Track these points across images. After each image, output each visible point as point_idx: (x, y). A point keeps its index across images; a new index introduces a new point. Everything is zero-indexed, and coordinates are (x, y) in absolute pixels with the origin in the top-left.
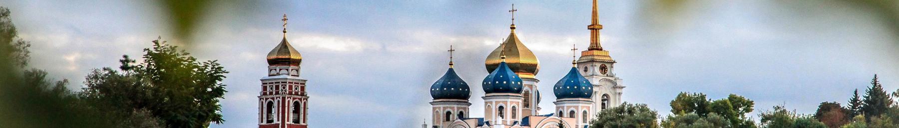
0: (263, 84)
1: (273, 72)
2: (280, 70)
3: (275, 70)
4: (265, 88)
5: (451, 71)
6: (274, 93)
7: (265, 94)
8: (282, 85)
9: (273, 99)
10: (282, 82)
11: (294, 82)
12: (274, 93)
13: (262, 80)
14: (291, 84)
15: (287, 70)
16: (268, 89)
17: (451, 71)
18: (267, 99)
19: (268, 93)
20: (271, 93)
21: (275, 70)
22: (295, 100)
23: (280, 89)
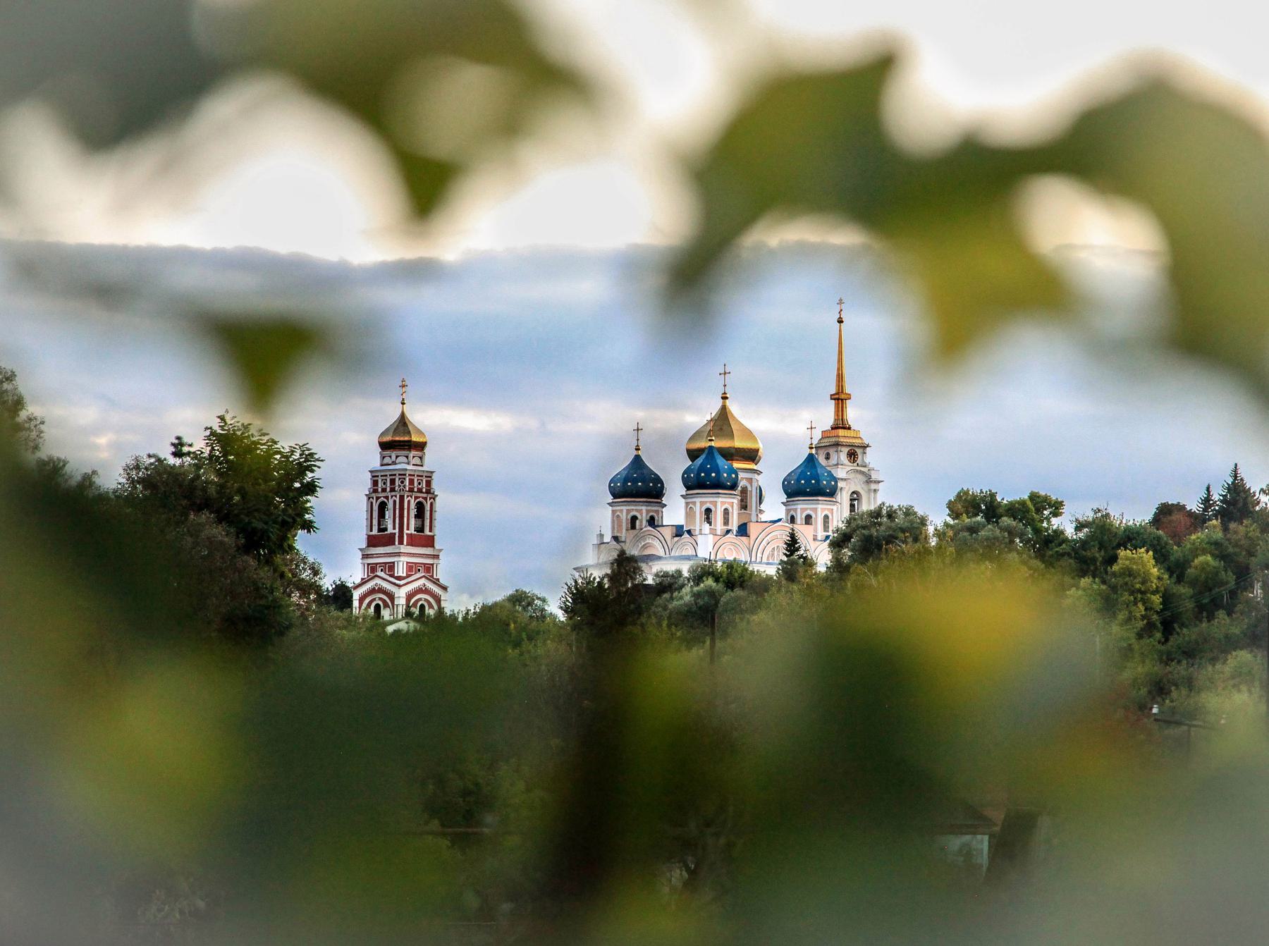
0: (373, 477)
1: (387, 460)
2: (397, 457)
3: (390, 457)
4: (375, 483)
5: (637, 459)
6: (388, 489)
7: (375, 491)
8: (399, 479)
9: (387, 498)
10: (400, 475)
11: (416, 474)
12: (388, 489)
13: (371, 472)
14: (412, 477)
15: (407, 457)
16: (380, 484)
17: (637, 459)
18: (378, 498)
19: (380, 490)
20: (384, 490)
21: (390, 457)
22: (418, 500)
23: (397, 484)
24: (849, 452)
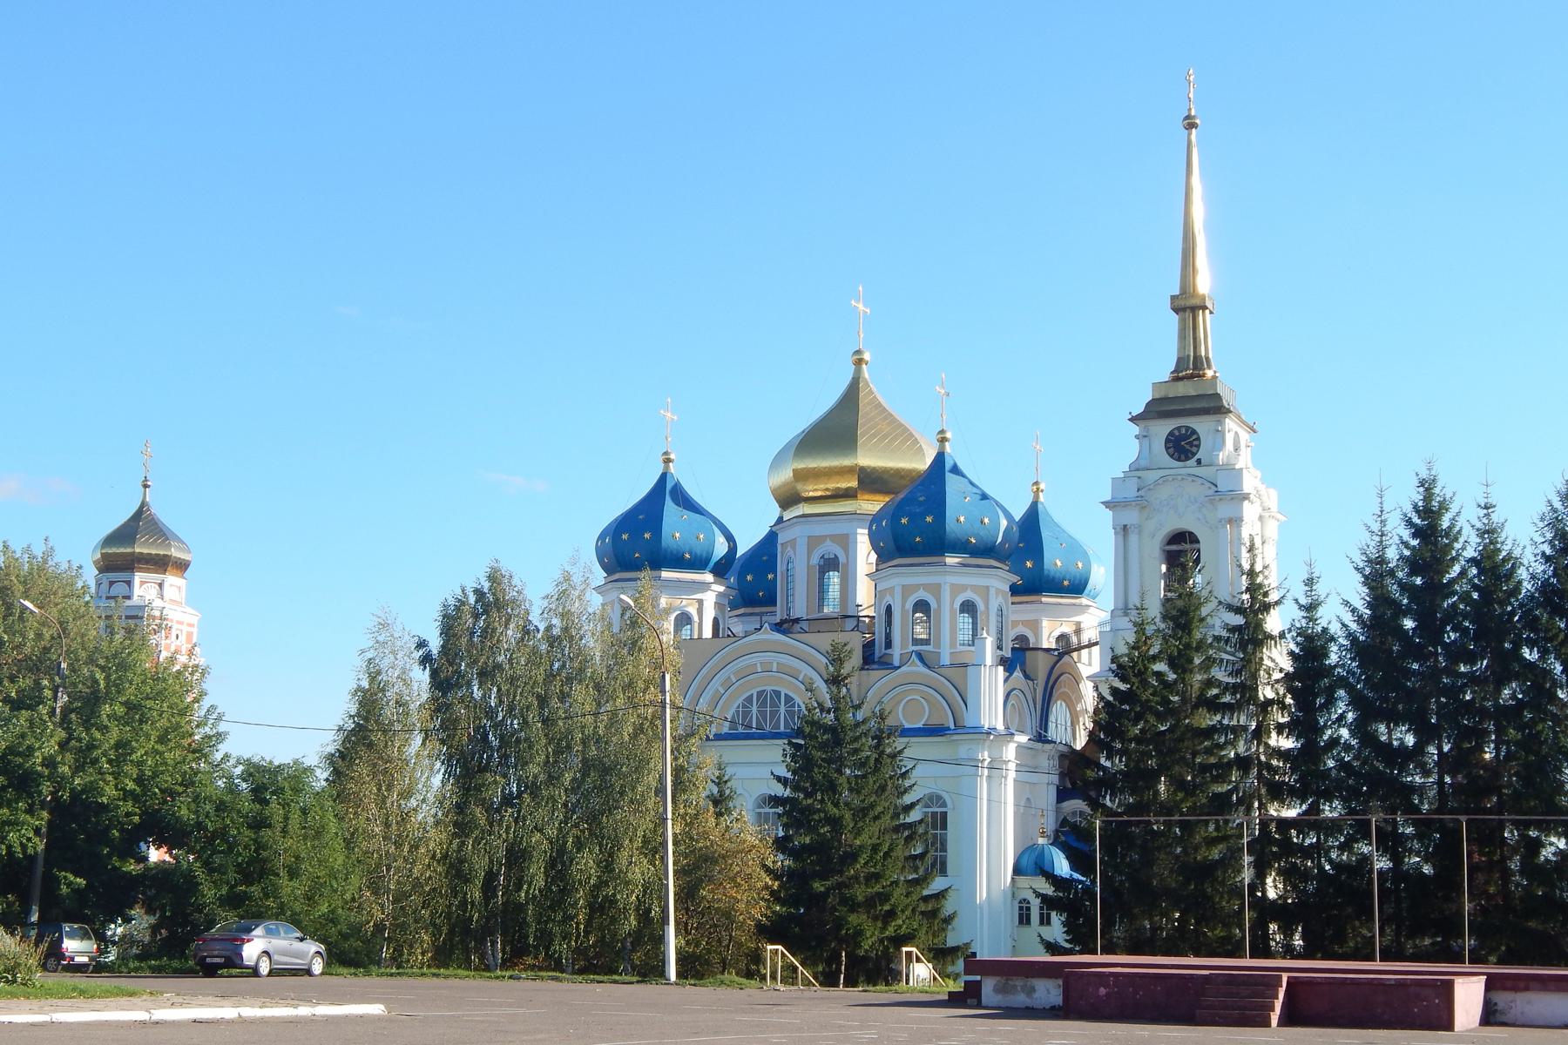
24: (1171, 434)
